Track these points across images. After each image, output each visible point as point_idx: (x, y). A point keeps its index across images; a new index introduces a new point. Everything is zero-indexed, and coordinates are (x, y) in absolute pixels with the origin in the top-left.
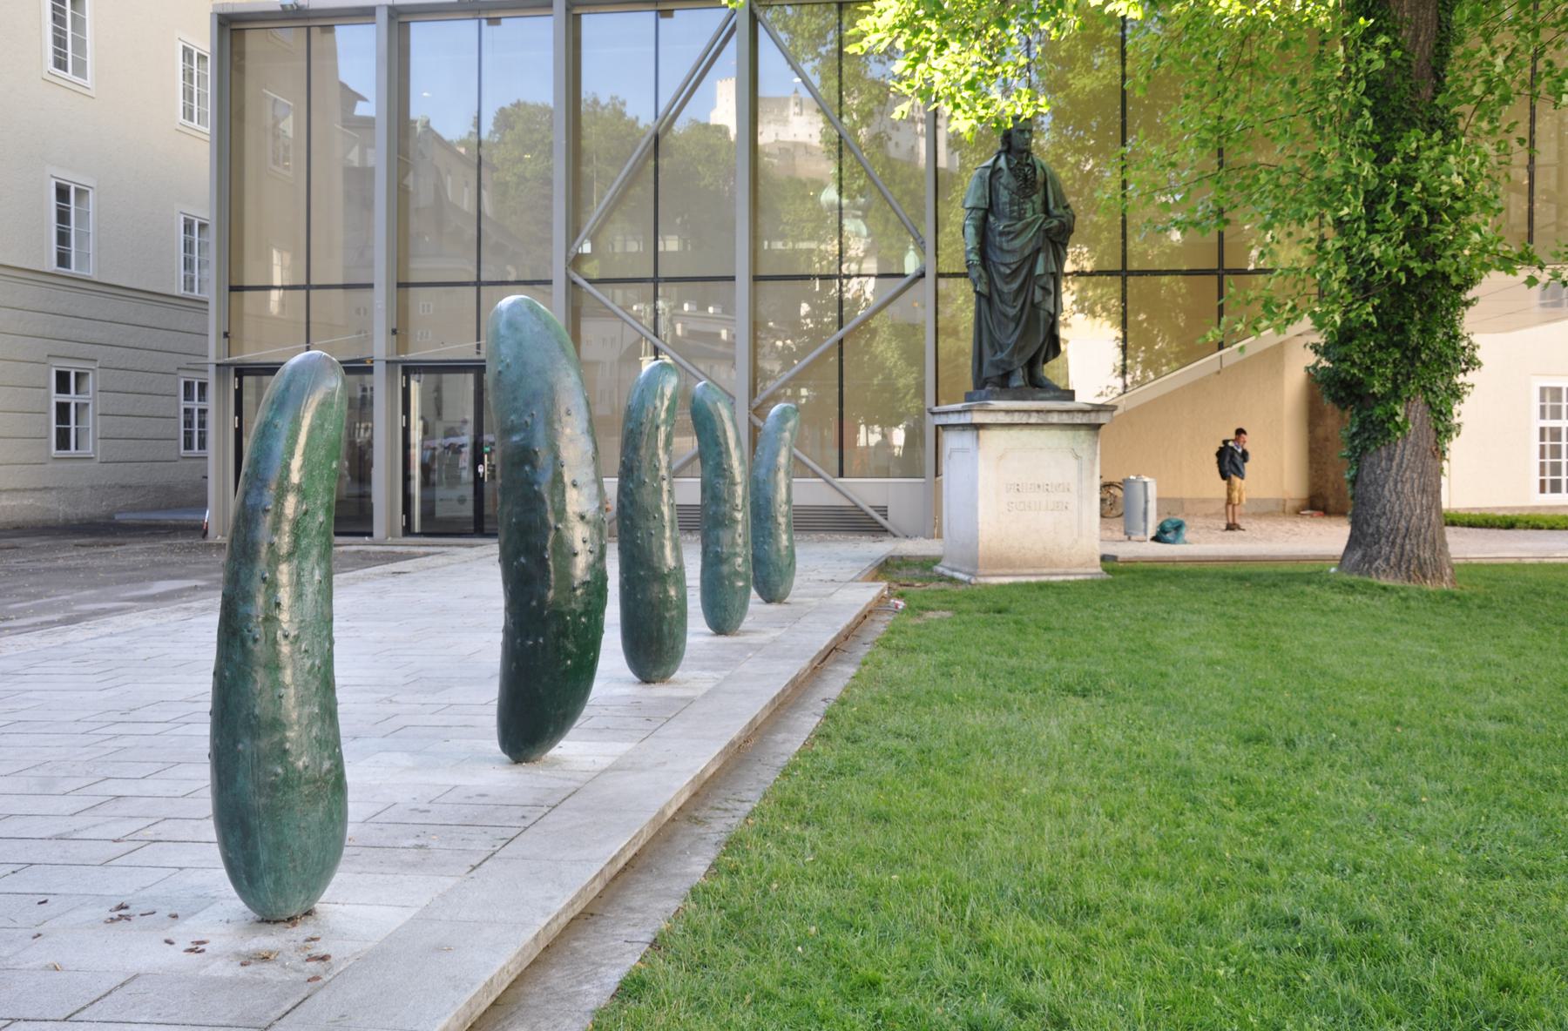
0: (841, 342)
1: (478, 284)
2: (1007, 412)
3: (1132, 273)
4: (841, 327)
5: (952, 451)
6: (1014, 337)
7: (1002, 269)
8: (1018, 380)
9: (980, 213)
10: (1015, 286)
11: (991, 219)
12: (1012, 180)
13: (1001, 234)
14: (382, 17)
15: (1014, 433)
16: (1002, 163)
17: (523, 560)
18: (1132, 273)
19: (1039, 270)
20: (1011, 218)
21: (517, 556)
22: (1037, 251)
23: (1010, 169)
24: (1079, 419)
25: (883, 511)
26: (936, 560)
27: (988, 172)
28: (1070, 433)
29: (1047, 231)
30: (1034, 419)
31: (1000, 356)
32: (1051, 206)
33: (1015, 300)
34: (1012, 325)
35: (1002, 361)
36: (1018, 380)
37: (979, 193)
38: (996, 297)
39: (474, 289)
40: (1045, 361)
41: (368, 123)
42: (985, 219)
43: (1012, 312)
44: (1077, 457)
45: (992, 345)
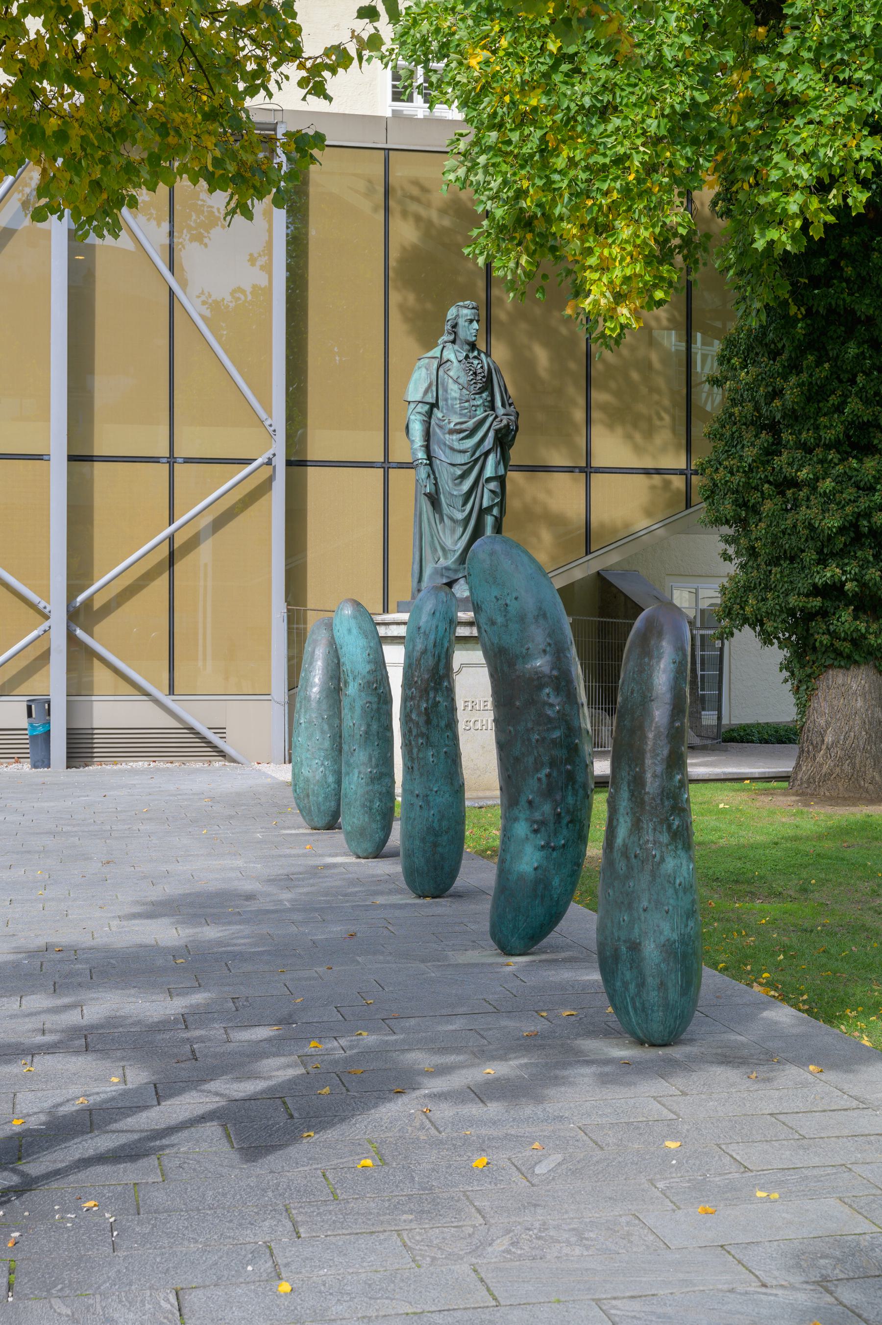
4: (171, 521)
7: (452, 469)
9: (427, 407)
12: (462, 374)
13: (451, 432)
19: (489, 472)
22: (487, 454)
25: (220, 731)
31: (443, 562)
33: (465, 504)
42: (430, 414)
43: (460, 516)
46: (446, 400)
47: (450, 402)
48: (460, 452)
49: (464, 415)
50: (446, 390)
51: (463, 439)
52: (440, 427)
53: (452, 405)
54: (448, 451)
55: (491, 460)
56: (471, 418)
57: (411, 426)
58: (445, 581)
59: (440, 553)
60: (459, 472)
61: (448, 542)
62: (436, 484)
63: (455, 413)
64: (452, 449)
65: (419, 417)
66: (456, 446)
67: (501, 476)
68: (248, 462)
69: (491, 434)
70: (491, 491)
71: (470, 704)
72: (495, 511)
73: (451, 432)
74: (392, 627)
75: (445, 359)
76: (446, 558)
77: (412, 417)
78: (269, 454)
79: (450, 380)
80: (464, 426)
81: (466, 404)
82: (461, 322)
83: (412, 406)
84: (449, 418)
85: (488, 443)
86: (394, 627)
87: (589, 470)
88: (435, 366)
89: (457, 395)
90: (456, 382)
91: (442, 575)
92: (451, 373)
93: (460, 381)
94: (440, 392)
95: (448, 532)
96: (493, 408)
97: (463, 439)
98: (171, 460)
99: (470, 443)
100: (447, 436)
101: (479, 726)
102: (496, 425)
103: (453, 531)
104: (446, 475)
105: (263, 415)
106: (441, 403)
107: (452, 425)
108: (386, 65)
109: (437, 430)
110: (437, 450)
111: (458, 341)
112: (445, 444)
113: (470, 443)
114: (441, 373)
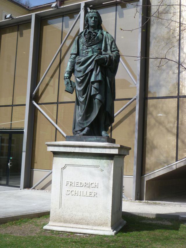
19: (92, 79)
22: (92, 71)
29: (96, 61)
69: (94, 63)
71: (70, 183)
101: (73, 193)
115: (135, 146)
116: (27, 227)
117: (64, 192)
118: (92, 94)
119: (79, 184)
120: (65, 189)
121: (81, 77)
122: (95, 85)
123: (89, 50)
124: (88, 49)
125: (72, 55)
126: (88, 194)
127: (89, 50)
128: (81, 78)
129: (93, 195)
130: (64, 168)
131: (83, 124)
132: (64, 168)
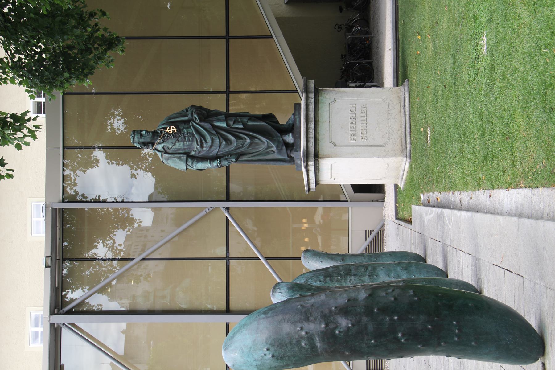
0: (267, 259)
1: (228, 259)
2: (308, 171)
3: (228, 31)
4: (258, 259)
5: (331, 177)
6: (264, 139)
7: (223, 146)
8: (289, 138)
9: (189, 160)
10: (233, 138)
11: (193, 153)
12: (170, 141)
13: (202, 146)
14: (59, 320)
15: (320, 137)
16: (160, 147)
17: (400, 335)
18: (228, 31)
19: (224, 125)
20: (193, 141)
21: (398, 340)
22: (214, 127)
23: (164, 142)
24: (312, 96)
25: (368, 233)
26: (396, 186)
27: (165, 155)
28: (320, 106)
29: (201, 121)
30: (312, 126)
31: (274, 149)
32: (186, 118)
33: (241, 138)
34: (256, 140)
35: (277, 147)
36: (289, 138)
37: (178, 161)
38: (239, 151)
39: (232, 262)
40: (278, 123)
41: (129, 325)
43: (248, 141)
44: (334, 101)
45: (268, 153)
46: (185, 149)
47: (186, 147)
48: (212, 142)
49: (193, 139)
50: (179, 149)
51: (206, 142)
52: (200, 152)
53: (187, 146)
54: (212, 149)
55: (218, 124)
56: (194, 136)
57: (199, 168)
58: (284, 148)
59: (269, 150)
60: (224, 142)
61: (264, 146)
62: (231, 155)
63: (191, 144)
64: (211, 146)
65: (194, 165)
66: (209, 144)
67: (226, 117)
68: (228, 220)
69: (202, 124)
70: (234, 123)
71: (353, 137)
72: (245, 120)
73: (202, 146)
74: (310, 177)
75: (162, 150)
76: (272, 147)
77: (195, 167)
78: (223, 210)
79: (174, 147)
80: (199, 140)
81: (187, 138)
82: (142, 140)
83: (188, 167)
84: (196, 148)
85: (207, 126)
86: (310, 181)
87: (228, 37)
88: (166, 155)
89: (182, 143)
90: (175, 144)
91: (281, 149)
92: (170, 147)
93: (174, 141)
94: (181, 152)
95: (257, 147)
96: (188, 122)
97: (206, 142)
98: (228, 37)
99: (208, 137)
100: (204, 149)
101: (364, 131)
102: (198, 121)
103: (257, 144)
104: (225, 148)
105: (203, 213)
106: (187, 151)
107: (198, 147)
108: (27, 144)
109: (201, 154)
110: (214, 152)
111: (153, 141)
112: (209, 150)
113: (208, 137)
114: (170, 152)
115: (313, 153)
116: (358, 84)
117: (364, 142)
118: (241, 126)
119: (352, 125)
120: (360, 141)
121: (219, 139)
122: (231, 123)
123: (186, 131)
124: (184, 134)
125: (188, 163)
126: (365, 114)
127: (186, 131)
128: (221, 139)
129: (365, 109)
130: (335, 145)
131: (279, 142)
132: (335, 145)
